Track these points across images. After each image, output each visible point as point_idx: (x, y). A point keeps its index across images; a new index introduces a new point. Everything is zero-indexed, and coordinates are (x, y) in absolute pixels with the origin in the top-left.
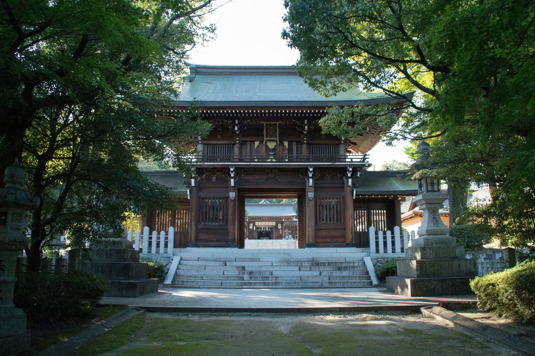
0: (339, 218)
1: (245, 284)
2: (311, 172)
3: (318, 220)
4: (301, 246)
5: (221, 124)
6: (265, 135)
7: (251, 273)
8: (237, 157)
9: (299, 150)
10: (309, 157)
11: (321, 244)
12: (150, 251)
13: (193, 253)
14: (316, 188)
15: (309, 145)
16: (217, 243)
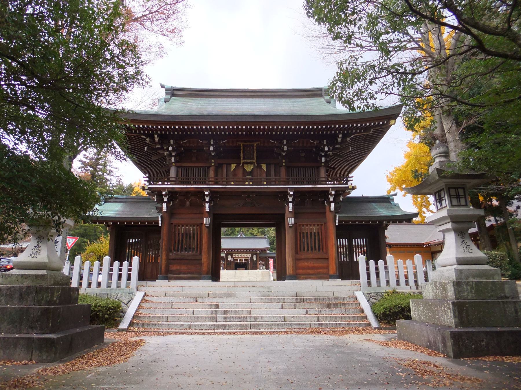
0: (321, 247)
1: (218, 327)
2: (291, 195)
3: (298, 249)
4: (281, 276)
5: (195, 145)
6: (242, 157)
7: (225, 312)
8: (213, 179)
9: (277, 173)
10: (288, 179)
11: (302, 276)
12: (109, 286)
13: (160, 287)
14: (296, 214)
15: (288, 168)
16: (189, 275)
